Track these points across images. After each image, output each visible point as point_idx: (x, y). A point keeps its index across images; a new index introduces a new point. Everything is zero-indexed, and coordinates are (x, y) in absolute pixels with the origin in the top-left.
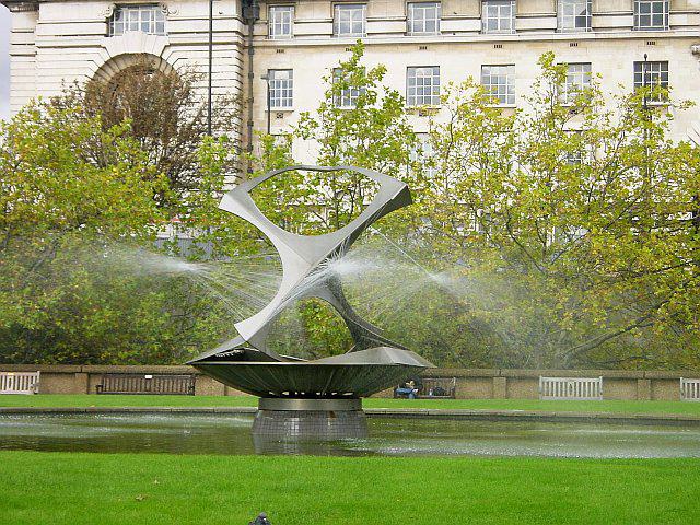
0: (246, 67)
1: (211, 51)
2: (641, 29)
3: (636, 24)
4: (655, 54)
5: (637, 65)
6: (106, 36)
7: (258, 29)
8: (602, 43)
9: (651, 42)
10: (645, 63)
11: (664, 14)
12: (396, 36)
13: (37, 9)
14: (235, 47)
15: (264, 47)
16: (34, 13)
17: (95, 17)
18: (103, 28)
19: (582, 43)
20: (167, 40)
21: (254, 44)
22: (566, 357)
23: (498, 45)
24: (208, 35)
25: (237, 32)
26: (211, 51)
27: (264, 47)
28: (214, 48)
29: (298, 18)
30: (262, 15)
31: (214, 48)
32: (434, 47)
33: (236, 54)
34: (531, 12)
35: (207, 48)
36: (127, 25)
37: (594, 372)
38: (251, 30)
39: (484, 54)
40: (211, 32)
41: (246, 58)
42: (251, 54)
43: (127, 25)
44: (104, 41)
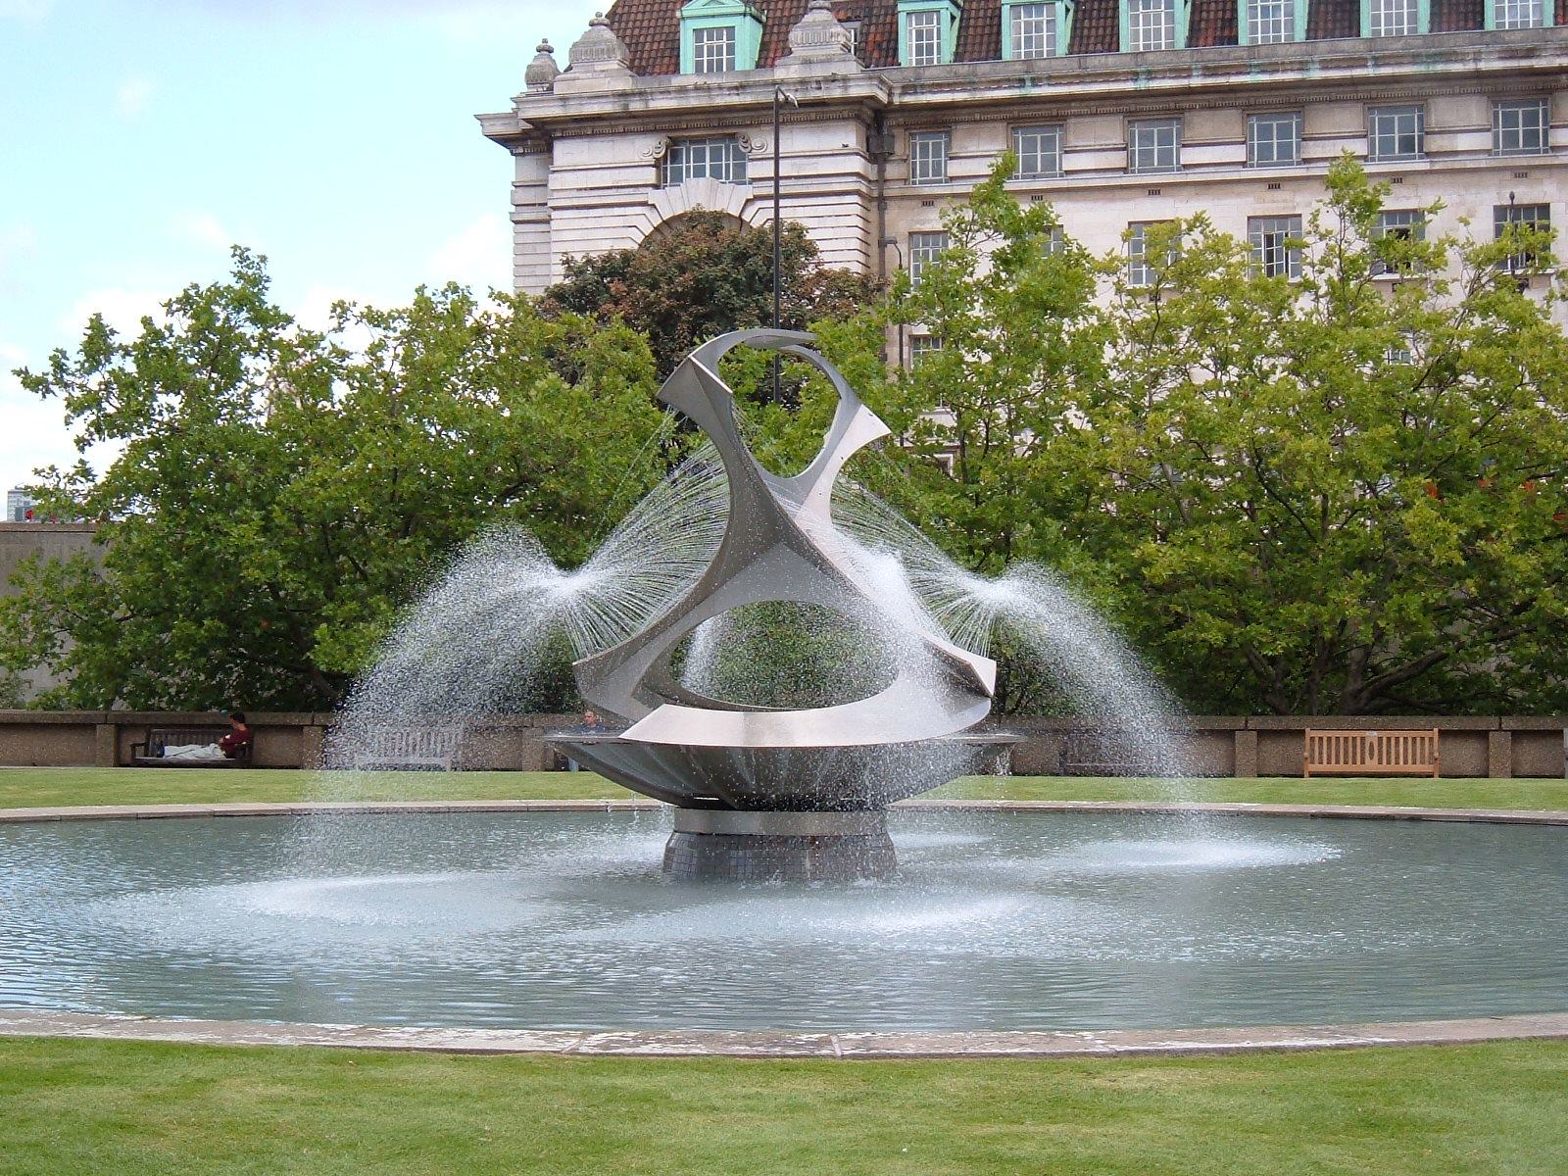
0: (874, 230)
1: (777, 208)
2: (1504, 153)
3: (1372, 151)
4: (1527, 193)
5: (1500, 212)
6: (656, 187)
7: (893, 170)
8: (1441, 178)
9: (1521, 173)
10: (1512, 206)
11: (1541, 127)
12: (1212, 169)
13: (550, 150)
14: (855, 199)
15: (902, 198)
16: (545, 156)
17: (637, 159)
18: (650, 176)
19: (1411, 179)
20: (749, 191)
21: (887, 193)
22: (1365, 694)
23: (1274, 184)
24: (772, 183)
25: (857, 174)
26: (777, 208)
27: (902, 198)
28: (782, 203)
29: (1308, 130)
30: (899, 148)
31: (782, 203)
32: (1293, 185)
33: (858, 209)
34: (1326, 130)
35: (772, 203)
36: (688, 168)
37: (1422, 720)
38: (881, 171)
39: (1251, 199)
40: (777, 178)
41: (874, 216)
42: (882, 209)
43: (688, 168)
44: (653, 196)
